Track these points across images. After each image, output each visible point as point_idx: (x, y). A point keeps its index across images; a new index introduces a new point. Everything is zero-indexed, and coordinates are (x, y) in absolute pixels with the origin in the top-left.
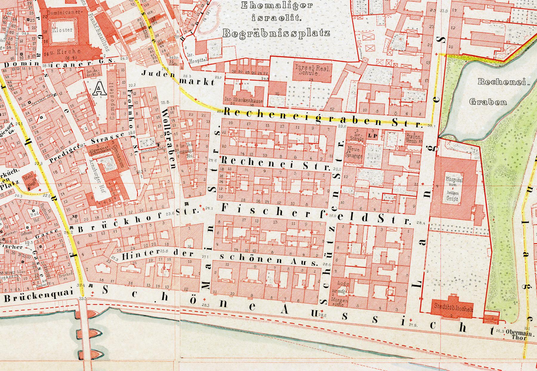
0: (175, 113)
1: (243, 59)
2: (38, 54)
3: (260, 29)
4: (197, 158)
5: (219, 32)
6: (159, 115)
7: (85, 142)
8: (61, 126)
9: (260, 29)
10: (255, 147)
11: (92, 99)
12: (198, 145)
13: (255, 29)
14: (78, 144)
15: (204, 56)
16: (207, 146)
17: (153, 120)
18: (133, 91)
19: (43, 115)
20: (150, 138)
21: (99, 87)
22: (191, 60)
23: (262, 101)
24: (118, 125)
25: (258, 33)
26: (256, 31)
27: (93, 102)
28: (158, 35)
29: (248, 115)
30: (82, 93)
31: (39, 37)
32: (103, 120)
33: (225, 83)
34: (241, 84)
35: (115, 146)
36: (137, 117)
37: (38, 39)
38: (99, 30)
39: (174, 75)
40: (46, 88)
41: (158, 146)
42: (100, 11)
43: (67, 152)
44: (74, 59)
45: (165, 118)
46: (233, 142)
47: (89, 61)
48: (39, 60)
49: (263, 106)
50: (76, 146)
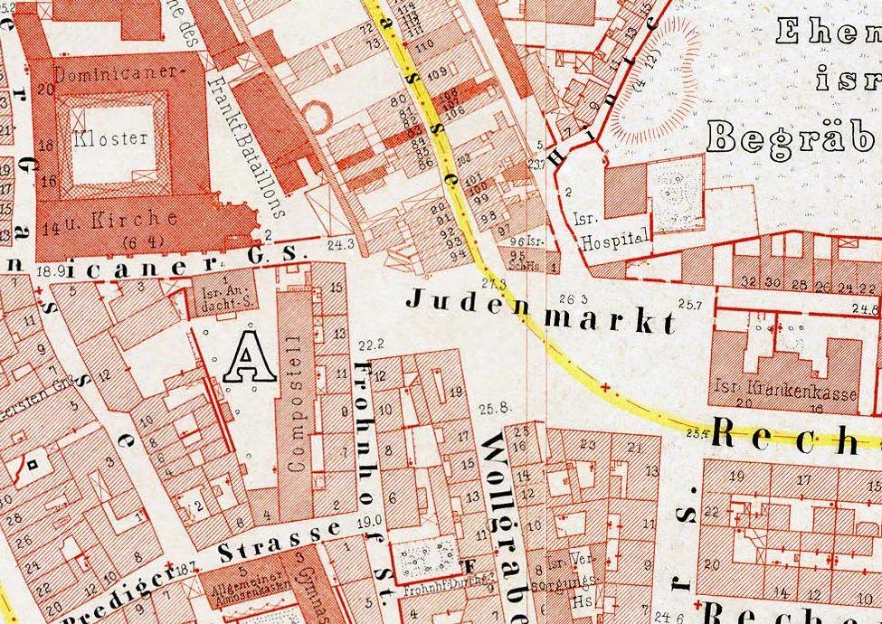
0: (532, 449)
1: (784, 233)
2: (18, 228)
3: (846, 121)
4: (609, 609)
5: (695, 135)
6: (471, 455)
7: (194, 556)
8: (106, 497)
9: (846, 121)
10: (829, 567)
11: (219, 398)
12: (614, 560)
13: (826, 123)
14: (169, 565)
15: (637, 224)
16: (649, 565)
17: (448, 474)
18: (375, 369)
19: (39, 455)
20: (439, 541)
21: (246, 351)
22: (587, 239)
23: (855, 395)
24: (317, 495)
25: (837, 136)
26: (833, 127)
27: (224, 409)
28: (466, 158)
29: (800, 446)
30: (182, 374)
31: (24, 164)
32: (259, 477)
33: (714, 326)
34: (775, 329)
35: (309, 572)
36: (389, 463)
37: (19, 172)
38: (248, 140)
39: (526, 305)
40: (49, 353)
41: (468, 571)
42: (252, 69)
43: (128, 593)
44: (153, 245)
45: (495, 465)
46: (745, 550)
47: (210, 255)
48: (25, 250)
49: (858, 414)
50: (162, 570)
